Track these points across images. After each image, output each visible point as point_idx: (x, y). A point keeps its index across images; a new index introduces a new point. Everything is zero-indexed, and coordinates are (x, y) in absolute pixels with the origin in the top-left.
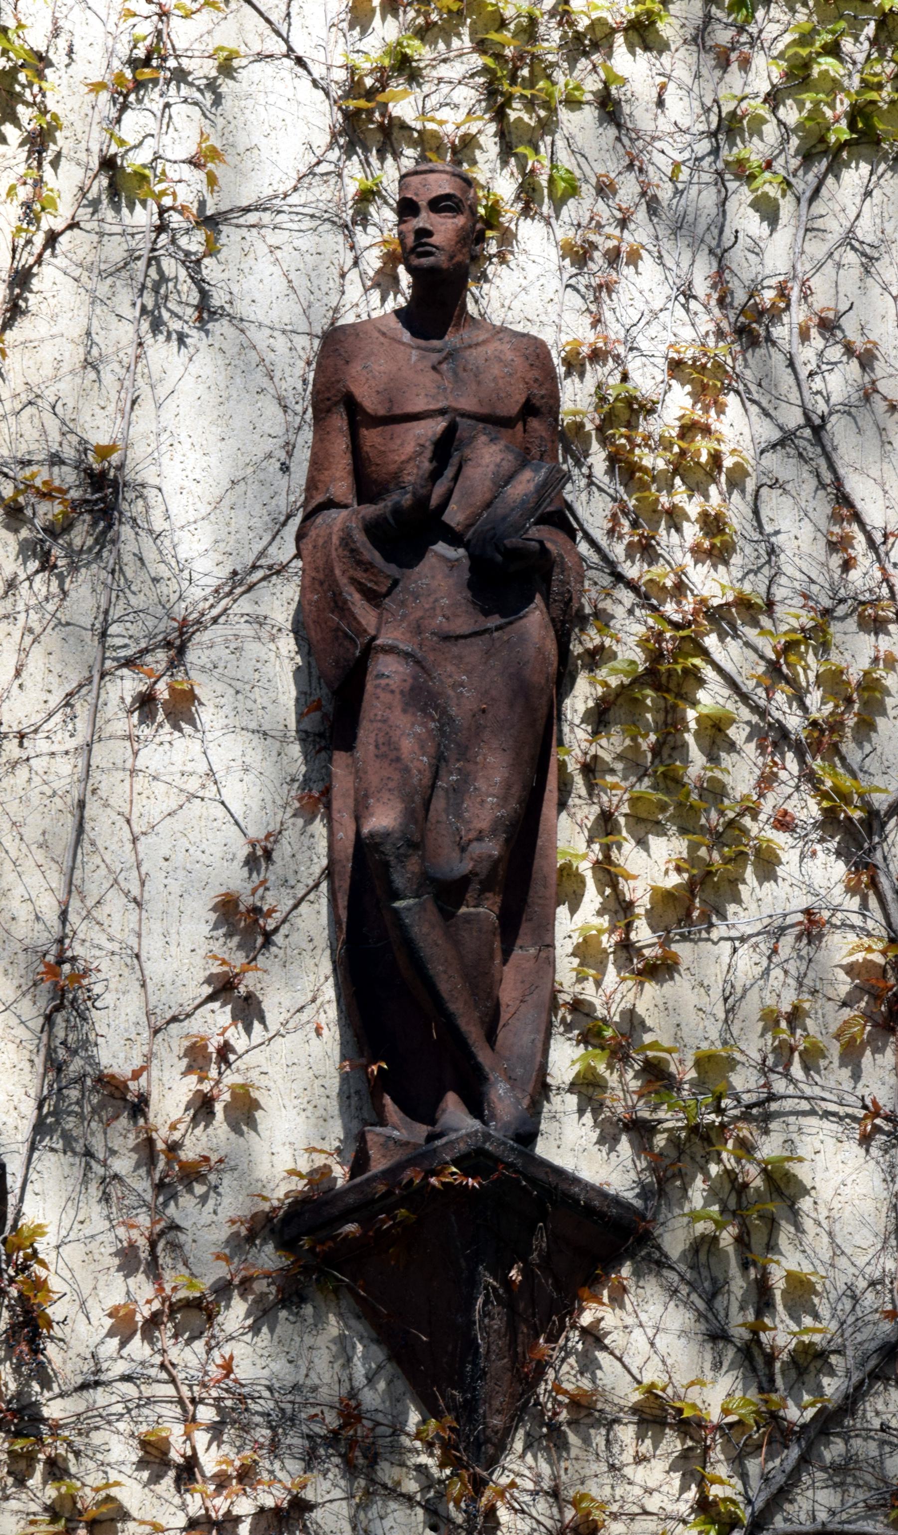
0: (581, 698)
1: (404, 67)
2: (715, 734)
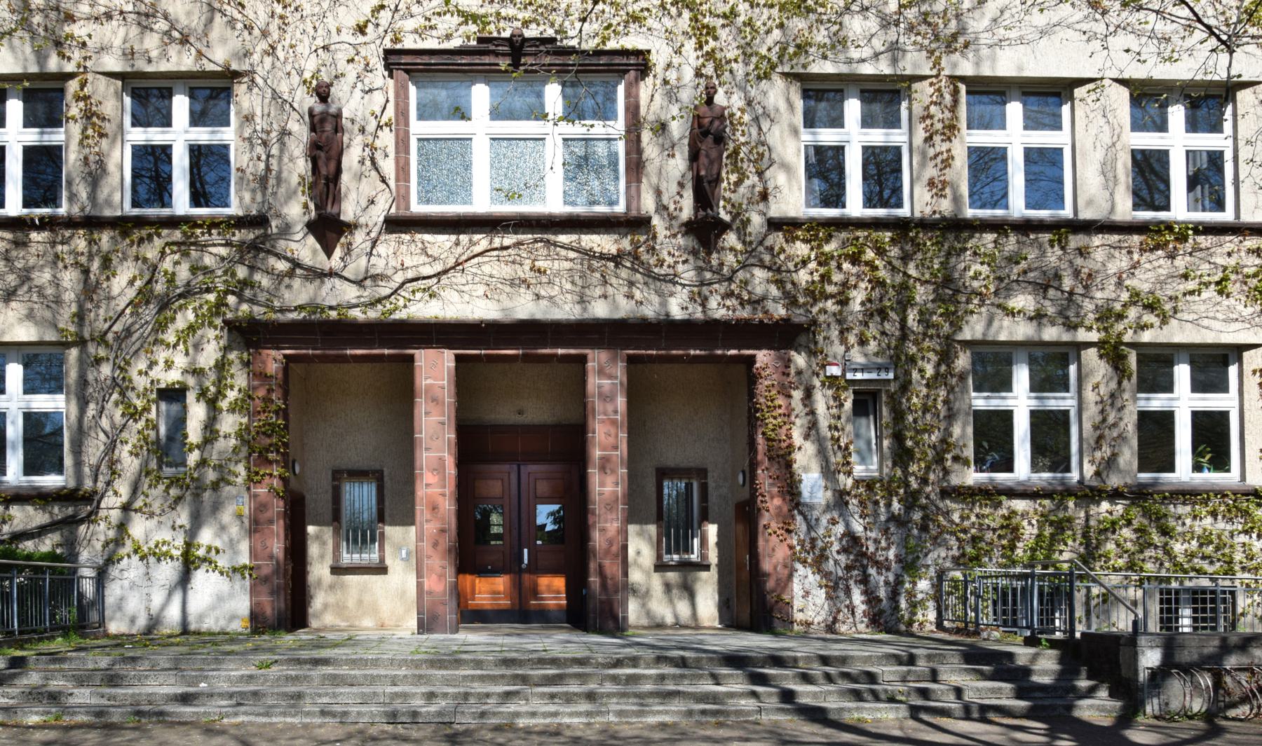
0: (725, 154)
1: (704, 66)
2: (742, 160)
